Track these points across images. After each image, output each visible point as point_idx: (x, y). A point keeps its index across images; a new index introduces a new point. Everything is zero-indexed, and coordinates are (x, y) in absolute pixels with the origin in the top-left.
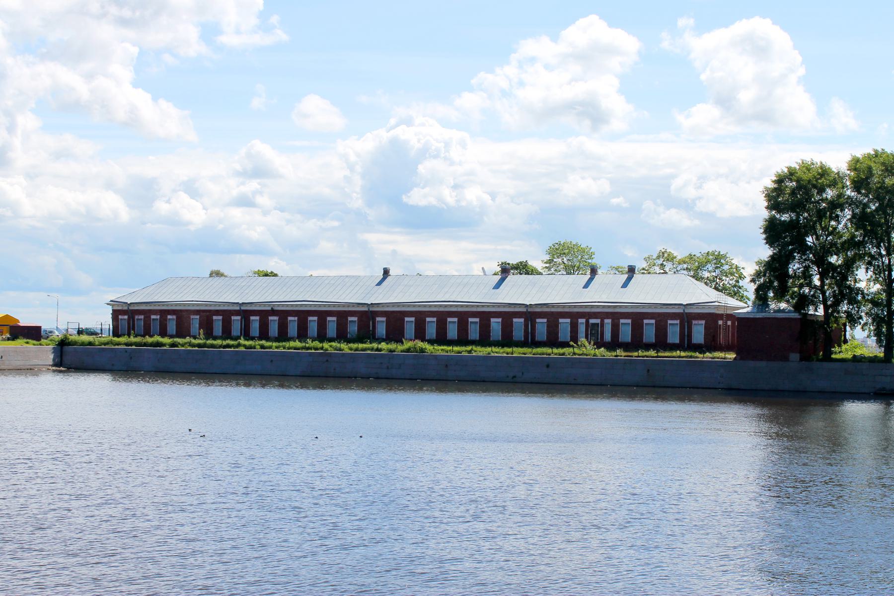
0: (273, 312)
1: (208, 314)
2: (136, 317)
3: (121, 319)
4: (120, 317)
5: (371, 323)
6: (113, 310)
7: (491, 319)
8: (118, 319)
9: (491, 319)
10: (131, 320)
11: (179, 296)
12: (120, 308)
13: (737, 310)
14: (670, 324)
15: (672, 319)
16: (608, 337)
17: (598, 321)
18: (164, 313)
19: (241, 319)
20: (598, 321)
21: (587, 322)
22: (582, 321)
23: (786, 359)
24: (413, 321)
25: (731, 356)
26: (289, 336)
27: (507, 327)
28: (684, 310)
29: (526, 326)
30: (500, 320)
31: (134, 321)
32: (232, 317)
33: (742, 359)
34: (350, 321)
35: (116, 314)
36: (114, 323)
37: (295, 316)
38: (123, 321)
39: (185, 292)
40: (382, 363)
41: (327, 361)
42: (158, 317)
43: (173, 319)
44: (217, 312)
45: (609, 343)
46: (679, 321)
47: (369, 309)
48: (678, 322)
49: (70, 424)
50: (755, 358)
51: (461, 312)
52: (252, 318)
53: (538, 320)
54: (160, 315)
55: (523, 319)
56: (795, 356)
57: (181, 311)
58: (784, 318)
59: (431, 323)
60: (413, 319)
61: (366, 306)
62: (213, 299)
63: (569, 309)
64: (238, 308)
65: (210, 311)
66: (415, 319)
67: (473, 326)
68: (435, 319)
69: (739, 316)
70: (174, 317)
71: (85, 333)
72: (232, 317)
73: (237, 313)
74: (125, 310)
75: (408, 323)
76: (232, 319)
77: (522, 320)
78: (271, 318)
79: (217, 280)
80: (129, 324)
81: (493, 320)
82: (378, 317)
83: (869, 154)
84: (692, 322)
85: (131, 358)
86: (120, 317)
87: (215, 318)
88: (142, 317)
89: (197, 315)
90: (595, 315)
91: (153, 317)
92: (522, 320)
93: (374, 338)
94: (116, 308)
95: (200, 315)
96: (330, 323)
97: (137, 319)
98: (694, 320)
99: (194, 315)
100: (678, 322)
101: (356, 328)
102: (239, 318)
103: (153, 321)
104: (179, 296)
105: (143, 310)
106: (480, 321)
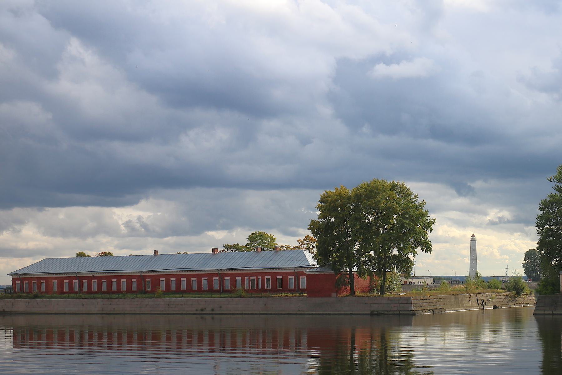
0: (94, 277)
1: (61, 279)
4: (16, 282)
5: (143, 281)
11: (182, 266)
12: (16, 277)
16: (260, 286)
17: (255, 278)
18: (39, 279)
20: (255, 278)
21: (249, 278)
23: (330, 296)
25: (306, 294)
26: (102, 290)
27: (285, 282)
29: (220, 281)
30: (207, 278)
31: (23, 284)
33: (309, 297)
35: (14, 280)
38: (162, 282)
39: (211, 263)
41: (110, 304)
44: (66, 278)
45: (260, 290)
47: (219, 273)
48: (293, 277)
49: (469, 301)
50: (315, 296)
53: (225, 278)
55: (218, 278)
58: (329, 274)
61: (217, 271)
62: (248, 265)
64: (217, 272)
66: (151, 280)
70: (44, 281)
72: (74, 280)
73: (76, 278)
79: (81, 259)
80: (21, 286)
81: (203, 278)
85: (13, 305)
87: (65, 281)
88: (28, 282)
89: (56, 280)
90: (253, 274)
91: (34, 281)
92: (217, 278)
96: (123, 283)
99: (54, 280)
100: (293, 277)
101: (136, 285)
102: (77, 281)
104: (178, 266)
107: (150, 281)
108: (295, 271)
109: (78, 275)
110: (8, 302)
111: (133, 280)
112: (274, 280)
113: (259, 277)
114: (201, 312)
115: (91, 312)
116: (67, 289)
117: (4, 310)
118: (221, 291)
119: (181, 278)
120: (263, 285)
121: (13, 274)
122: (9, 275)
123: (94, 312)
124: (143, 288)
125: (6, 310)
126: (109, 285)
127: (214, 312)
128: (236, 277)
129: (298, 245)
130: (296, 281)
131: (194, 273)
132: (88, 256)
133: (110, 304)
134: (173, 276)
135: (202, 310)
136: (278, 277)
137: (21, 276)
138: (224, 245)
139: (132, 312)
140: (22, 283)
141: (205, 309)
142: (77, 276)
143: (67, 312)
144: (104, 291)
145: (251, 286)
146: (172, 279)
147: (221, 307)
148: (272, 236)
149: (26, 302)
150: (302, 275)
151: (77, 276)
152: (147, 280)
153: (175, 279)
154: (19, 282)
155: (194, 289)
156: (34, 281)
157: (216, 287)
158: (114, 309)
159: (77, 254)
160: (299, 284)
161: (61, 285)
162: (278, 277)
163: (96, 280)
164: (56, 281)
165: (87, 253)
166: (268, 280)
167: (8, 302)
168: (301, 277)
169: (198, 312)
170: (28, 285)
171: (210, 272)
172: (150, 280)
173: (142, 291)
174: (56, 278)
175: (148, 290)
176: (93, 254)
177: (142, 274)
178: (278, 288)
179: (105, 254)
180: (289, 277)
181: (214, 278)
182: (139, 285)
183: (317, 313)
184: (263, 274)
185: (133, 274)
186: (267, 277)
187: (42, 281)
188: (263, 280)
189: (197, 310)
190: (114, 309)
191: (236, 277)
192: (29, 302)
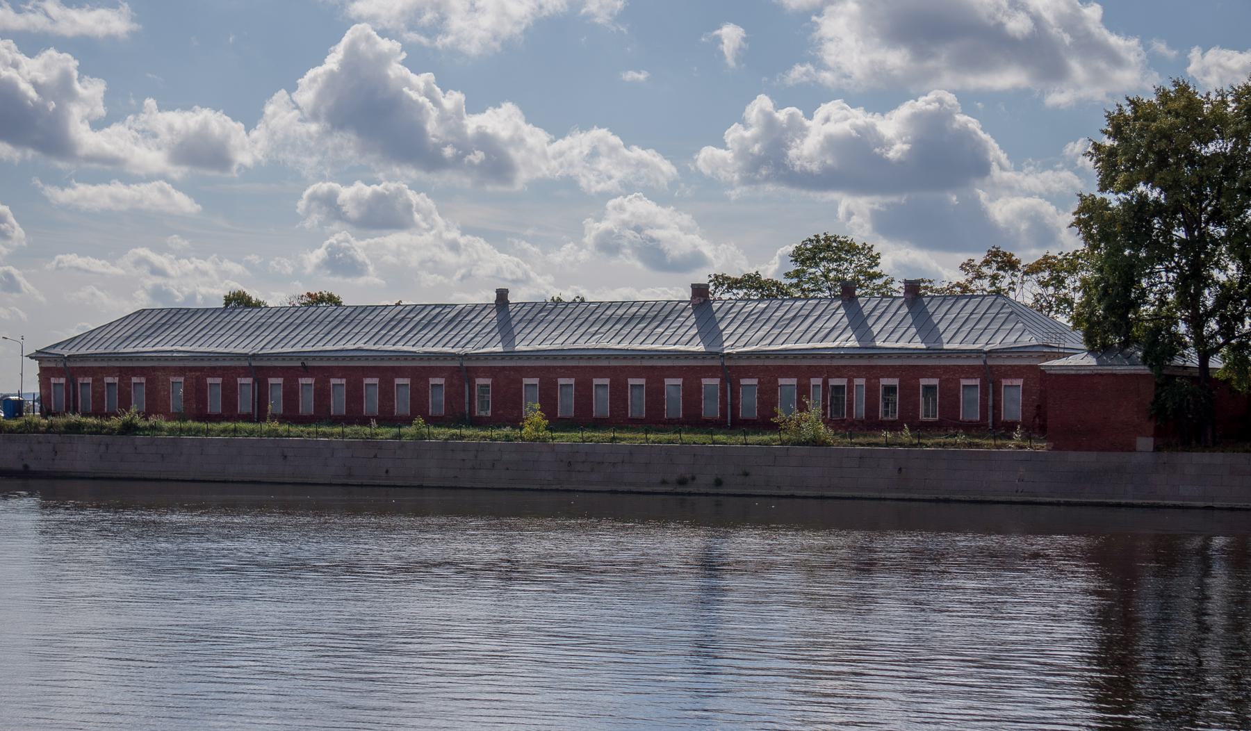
0: (306, 371)
1: (198, 374)
2: (80, 380)
3: (54, 384)
4: (53, 380)
6: (41, 368)
7: (665, 380)
8: (50, 384)
9: (665, 380)
10: (71, 386)
12: (52, 365)
13: (1054, 358)
14: (964, 386)
15: (967, 378)
16: (860, 410)
17: (842, 382)
18: (125, 373)
19: (253, 383)
20: (842, 382)
21: (825, 383)
22: (817, 381)
23: (1131, 448)
24: (218, 384)
26: (332, 413)
27: (197, 393)
28: (985, 362)
30: (679, 381)
31: (997, 392)
32: (238, 379)
34: (432, 385)
35: (45, 374)
36: (43, 391)
37: (341, 378)
40: (464, 460)
41: (375, 457)
42: (116, 380)
43: (141, 384)
44: (213, 371)
46: (978, 380)
48: (977, 382)
51: (415, 368)
52: (272, 381)
53: (744, 382)
54: (119, 376)
56: (1145, 443)
57: (154, 369)
58: (1130, 375)
59: (177, 388)
60: (536, 381)
63: (794, 361)
65: (202, 369)
67: (600, 392)
68: (572, 381)
69: (1052, 372)
70: (143, 380)
71: (63, 429)
72: (238, 379)
73: (246, 371)
74: (60, 368)
75: (400, 389)
76: (239, 382)
77: (717, 381)
78: (302, 381)
81: (668, 381)
82: (478, 377)
83: (250, 298)
84: (1001, 382)
86: (53, 380)
87: (210, 380)
89: (1017, 377)
90: (838, 371)
91: (108, 380)
92: (717, 381)
93: (365, 421)
94: (46, 365)
95: (185, 375)
97: (81, 384)
98: (1004, 378)
100: (977, 382)
102: (249, 380)
103: (631, 389)
105: (92, 368)
106: (647, 383)
107: (488, 386)
108: (985, 362)
109: (254, 364)
110: (40, 443)
111: (433, 381)
112: (909, 392)
113: (526, 379)
114: (680, 489)
115: (310, 481)
116: (215, 404)
117: (26, 466)
118: (726, 422)
119: (594, 380)
120: (871, 407)
121: (43, 355)
122: (31, 358)
123: (321, 481)
124: (467, 408)
125: (34, 466)
126: (355, 394)
127: (721, 491)
128: (779, 380)
129: (962, 278)
130: (987, 395)
131: (638, 363)
132: (258, 305)
133: (375, 457)
134: (568, 371)
135: (682, 482)
136: (924, 382)
137: (69, 360)
138: (710, 276)
139: (447, 484)
140: (72, 383)
141: (693, 478)
142: (250, 364)
143: (230, 478)
144: (337, 414)
145: (831, 410)
146: (561, 381)
147: (746, 474)
148: (869, 248)
149: (100, 444)
150: (1007, 376)
151: (250, 364)
152: (480, 381)
153: (572, 381)
154: (63, 380)
155: (636, 415)
156: (108, 380)
157: (710, 409)
158: (387, 472)
159: (226, 297)
160: (997, 407)
161: (197, 393)
162: (924, 382)
163: (310, 381)
164: (182, 379)
165: (255, 295)
166: (890, 390)
167: (40, 443)
168: (1005, 382)
169: (669, 489)
170: (279, 393)
171: (583, 363)
172: (488, 381)
173: (458, 416)
174: (181, 371)
175: (483, 413)
176: (275, 298)
177: (466, 364)
178: (922, 417)
179: (316, 300)
180: (964, 382)
181: (781, 381)
182: (454, 395)
183: (1084, 500)
184: (872, 373)
185: (433, 364)
186: (885, 381)
187: (135, 380)
188: (871, 390)
189: (664, 482)
190: (387, 472)
191: (779, 380)
192: (107, 446)
